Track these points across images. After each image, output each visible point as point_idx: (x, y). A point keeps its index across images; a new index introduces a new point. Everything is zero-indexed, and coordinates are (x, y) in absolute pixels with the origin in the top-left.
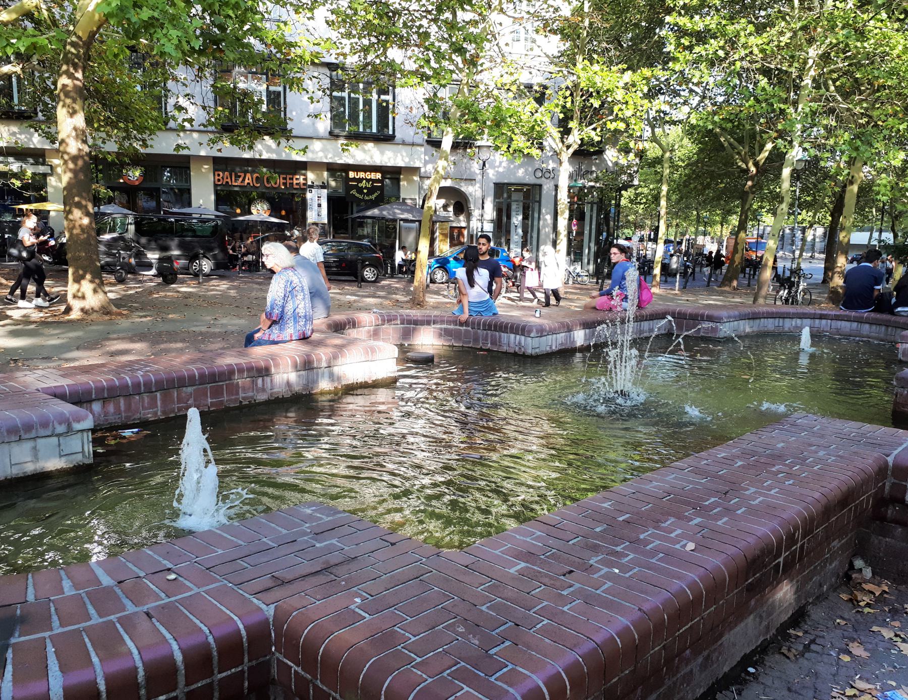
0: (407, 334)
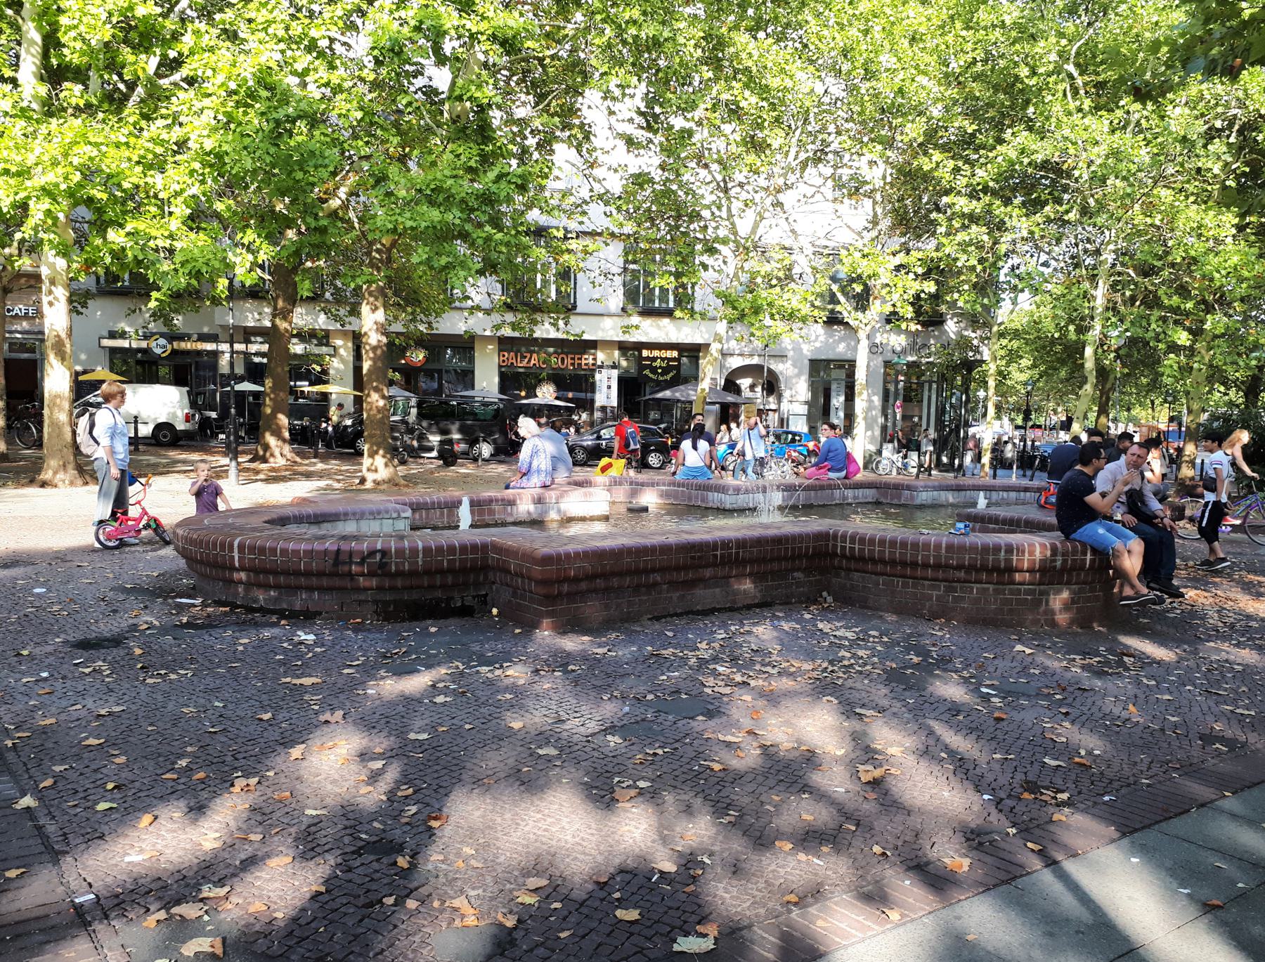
0: (634, 493)
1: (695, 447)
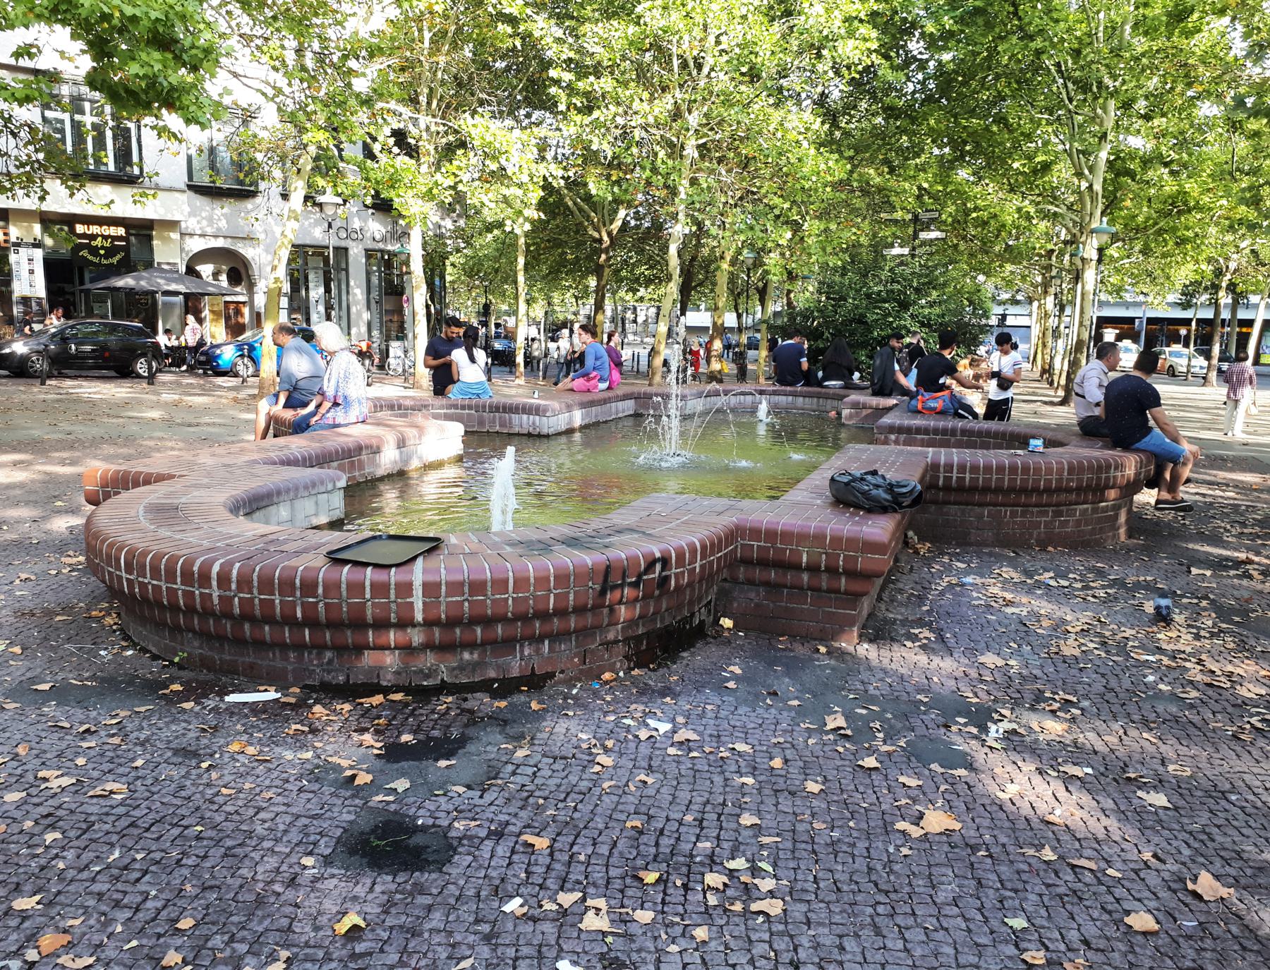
1: (472, 359)
